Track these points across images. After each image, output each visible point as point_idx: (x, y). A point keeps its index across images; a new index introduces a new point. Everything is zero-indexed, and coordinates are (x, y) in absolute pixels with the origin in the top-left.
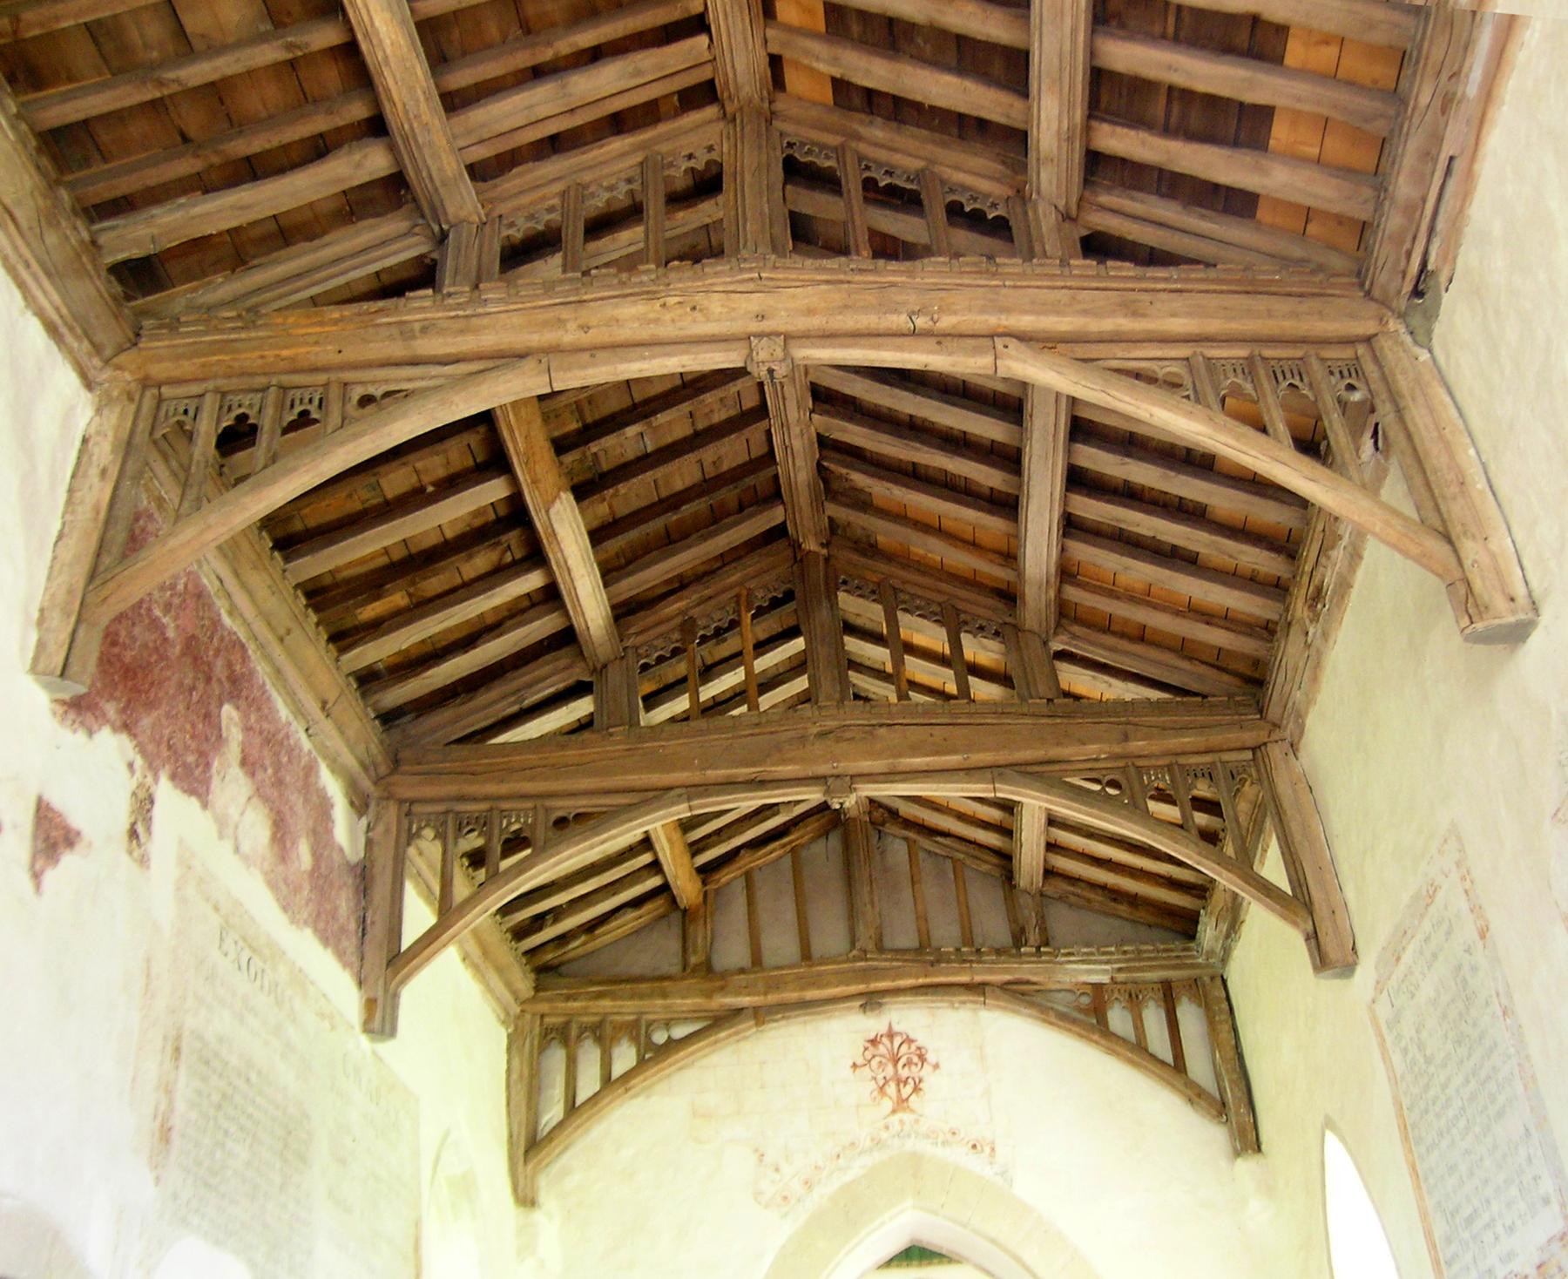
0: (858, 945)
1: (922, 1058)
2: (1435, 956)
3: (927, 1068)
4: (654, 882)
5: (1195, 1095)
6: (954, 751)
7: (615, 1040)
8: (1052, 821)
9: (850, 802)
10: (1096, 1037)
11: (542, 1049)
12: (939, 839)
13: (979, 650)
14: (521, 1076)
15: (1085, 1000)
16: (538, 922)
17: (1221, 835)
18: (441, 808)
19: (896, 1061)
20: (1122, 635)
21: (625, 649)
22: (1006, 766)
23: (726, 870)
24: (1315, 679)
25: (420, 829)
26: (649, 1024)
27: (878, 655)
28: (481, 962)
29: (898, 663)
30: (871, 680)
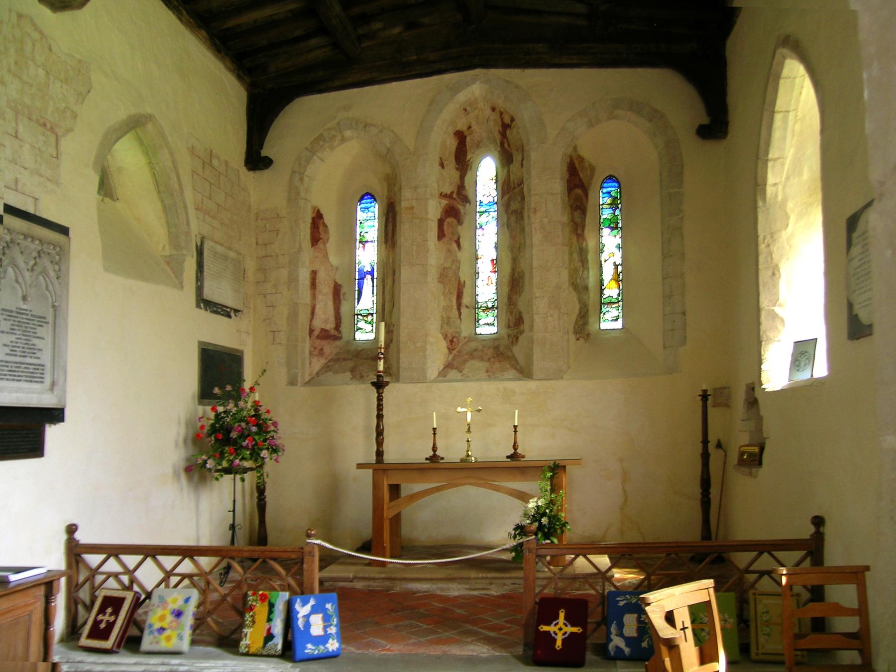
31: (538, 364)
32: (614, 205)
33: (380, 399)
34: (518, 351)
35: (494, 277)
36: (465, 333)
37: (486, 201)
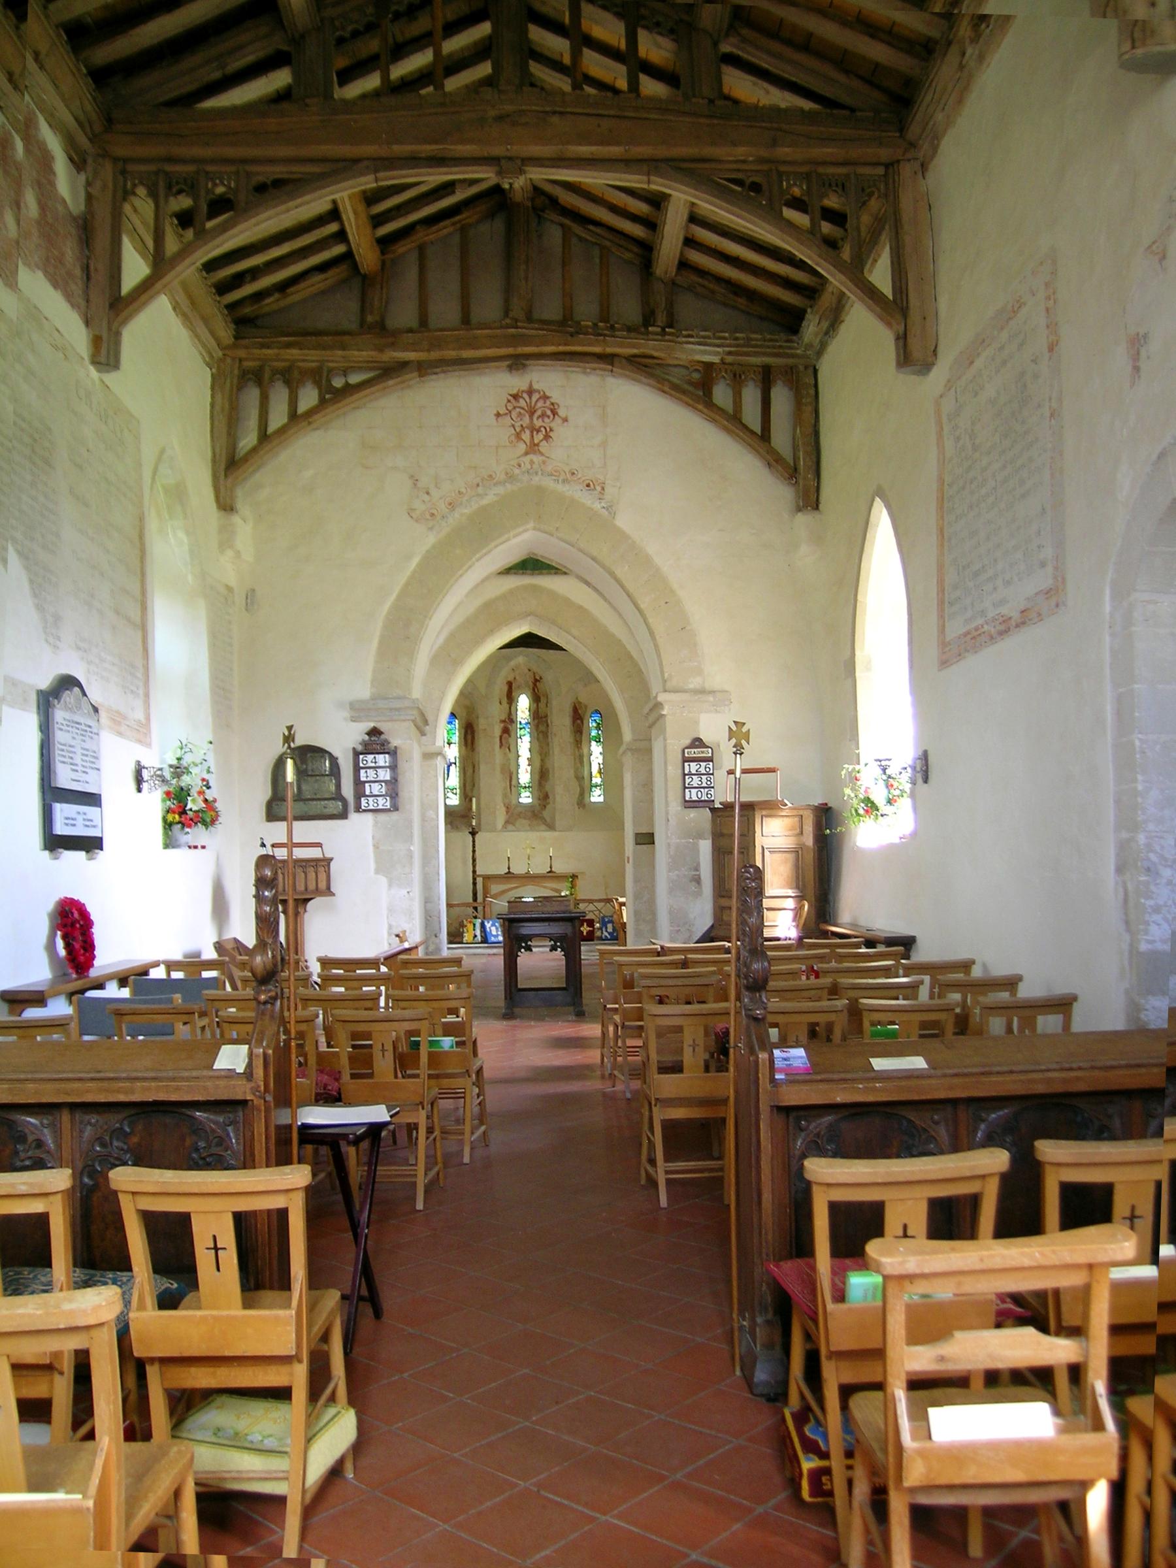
0: (511, 314)
1: (554, 413)
2: (1004, 363)
3: (558, 420)
4: (339, 249)
5: (774, 460)
6: (618, 144)
7: (301, 382)
8: (694, 219)
9: (518, 184)
10: (700, 407)
11: (240, 388)
12: (591, 227)
13: (654, 48)
14: (223, 410)
15: (696, 376)
16: (238, 280)
17: (840, 243)
18: (152, 168)
19: (532, 413)
20: (789, 42)
21: (322, 20)
22: (662, 160)
23: (402, 243)
24: (960, 101)
25: (135, 185)
26: (330, 371)
27: (557, 45)
28: (188, 312)
29: (576, 54)
30: (547, 70)
31: (558, 824)
32: (598, 728)
33: (474, 841)
34: (546, 814)
35: (529, 768)
36: (514, 802)
37: (523, 722)
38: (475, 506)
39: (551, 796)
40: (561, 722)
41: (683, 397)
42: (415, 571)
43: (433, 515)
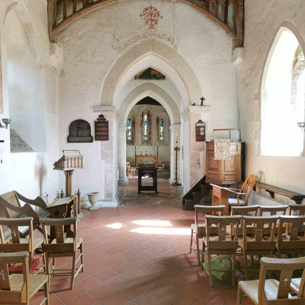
1: (158, 15)
36: (143, 139)
38: (133, 45)
39: (151, 138)
40: (154, 122)
41: (200, 9)
42: (114, 66)
43: (120, 48)
